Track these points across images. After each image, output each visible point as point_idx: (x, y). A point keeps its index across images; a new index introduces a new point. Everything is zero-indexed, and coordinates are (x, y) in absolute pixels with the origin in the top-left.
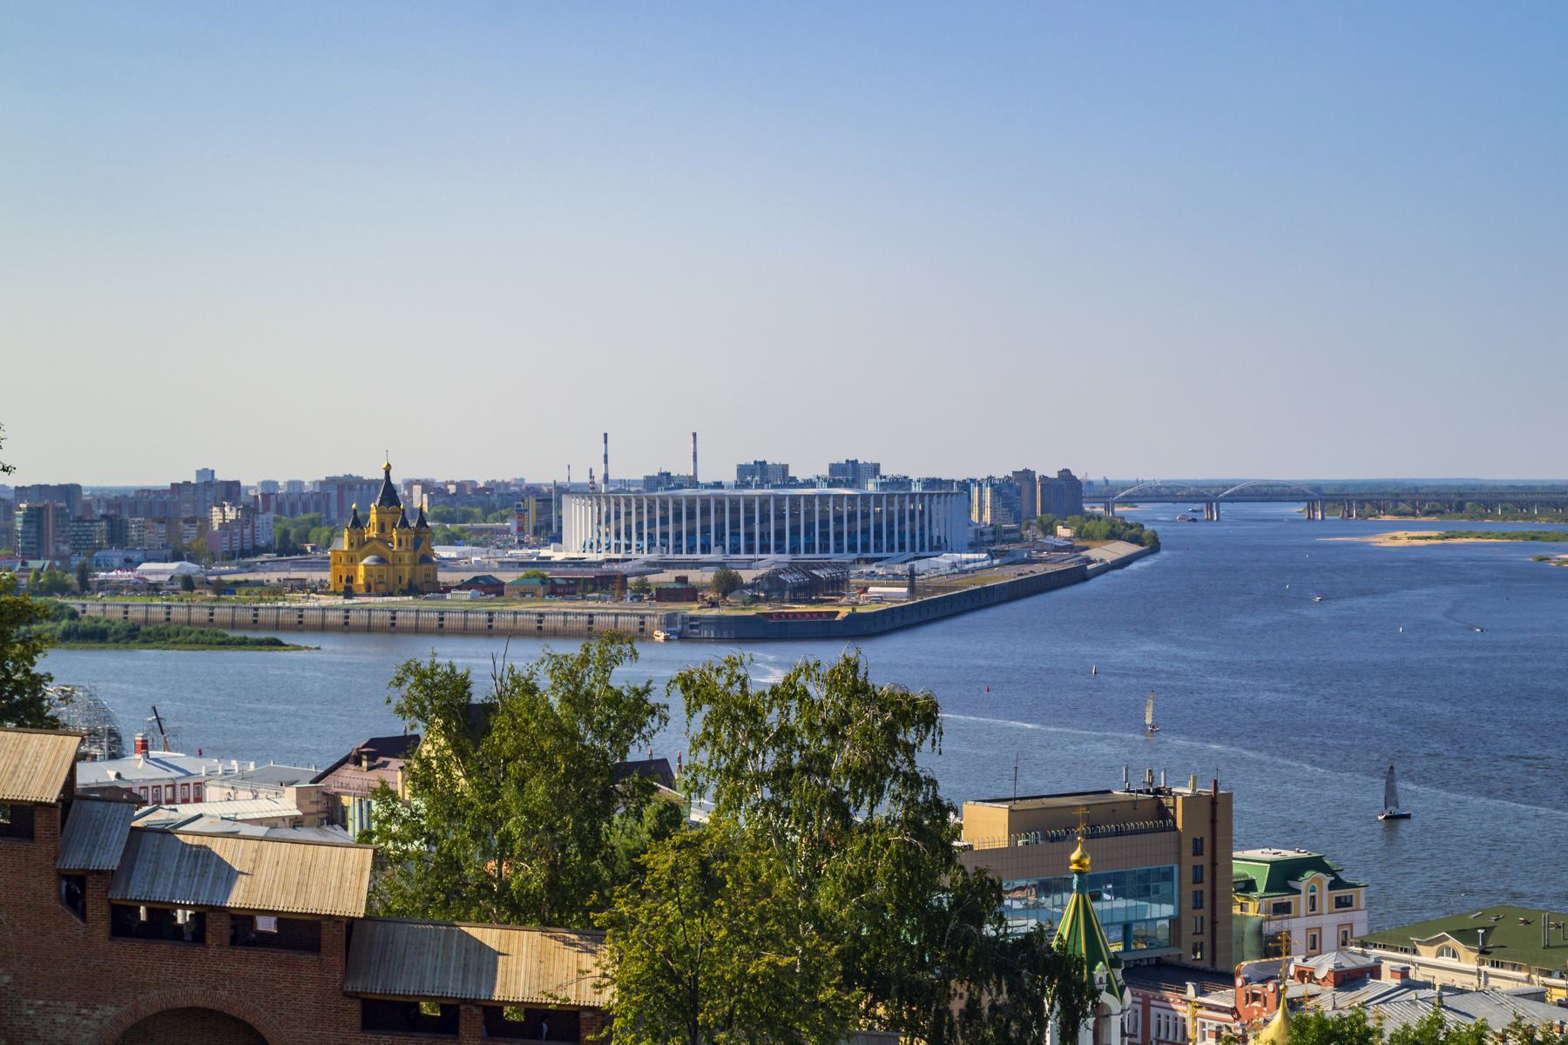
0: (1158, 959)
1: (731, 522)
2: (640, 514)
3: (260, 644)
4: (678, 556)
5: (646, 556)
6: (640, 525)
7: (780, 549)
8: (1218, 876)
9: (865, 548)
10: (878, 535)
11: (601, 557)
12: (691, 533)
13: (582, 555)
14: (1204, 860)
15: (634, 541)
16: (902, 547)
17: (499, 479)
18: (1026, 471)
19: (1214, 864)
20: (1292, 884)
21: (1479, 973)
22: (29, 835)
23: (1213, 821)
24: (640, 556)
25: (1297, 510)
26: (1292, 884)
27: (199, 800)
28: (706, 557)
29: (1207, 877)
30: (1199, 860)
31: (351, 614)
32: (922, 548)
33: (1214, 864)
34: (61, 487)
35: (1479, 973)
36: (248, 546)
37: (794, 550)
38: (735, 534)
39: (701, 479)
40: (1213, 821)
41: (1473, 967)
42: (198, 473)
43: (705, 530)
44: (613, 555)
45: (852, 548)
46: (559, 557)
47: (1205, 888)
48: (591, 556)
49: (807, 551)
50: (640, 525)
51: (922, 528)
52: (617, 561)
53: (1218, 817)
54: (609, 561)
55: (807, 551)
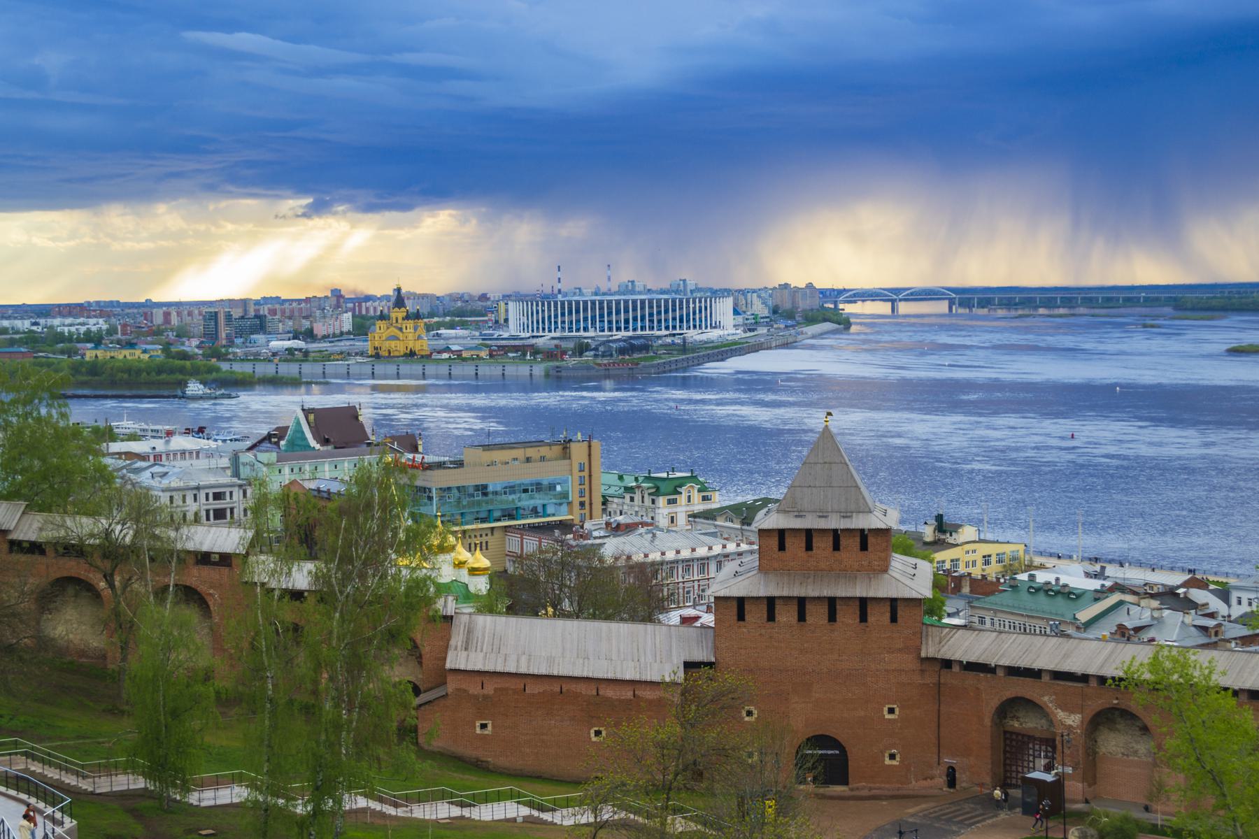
2: (549, 310)
3: (168, 397)
5: (553, 334)
7: (626, 328)
9: (674, 328)
10: (681, 321)
12: (578, 321)
14: (586, 474)
16: (695, 327)
17: (91, 300)
19: (590, 476)
22: (230, 565)
23: (590, 455)
25: (943, 307)
29: (587, 482)
33: (590, 476)
36: (337, 332)
37: (635, 330)
38: (602, 321)
40: (590, 455)
45: (667, 328)
46: (506, 335)
47: (586, 487)
48: (523, 335)
50: (550, 317)
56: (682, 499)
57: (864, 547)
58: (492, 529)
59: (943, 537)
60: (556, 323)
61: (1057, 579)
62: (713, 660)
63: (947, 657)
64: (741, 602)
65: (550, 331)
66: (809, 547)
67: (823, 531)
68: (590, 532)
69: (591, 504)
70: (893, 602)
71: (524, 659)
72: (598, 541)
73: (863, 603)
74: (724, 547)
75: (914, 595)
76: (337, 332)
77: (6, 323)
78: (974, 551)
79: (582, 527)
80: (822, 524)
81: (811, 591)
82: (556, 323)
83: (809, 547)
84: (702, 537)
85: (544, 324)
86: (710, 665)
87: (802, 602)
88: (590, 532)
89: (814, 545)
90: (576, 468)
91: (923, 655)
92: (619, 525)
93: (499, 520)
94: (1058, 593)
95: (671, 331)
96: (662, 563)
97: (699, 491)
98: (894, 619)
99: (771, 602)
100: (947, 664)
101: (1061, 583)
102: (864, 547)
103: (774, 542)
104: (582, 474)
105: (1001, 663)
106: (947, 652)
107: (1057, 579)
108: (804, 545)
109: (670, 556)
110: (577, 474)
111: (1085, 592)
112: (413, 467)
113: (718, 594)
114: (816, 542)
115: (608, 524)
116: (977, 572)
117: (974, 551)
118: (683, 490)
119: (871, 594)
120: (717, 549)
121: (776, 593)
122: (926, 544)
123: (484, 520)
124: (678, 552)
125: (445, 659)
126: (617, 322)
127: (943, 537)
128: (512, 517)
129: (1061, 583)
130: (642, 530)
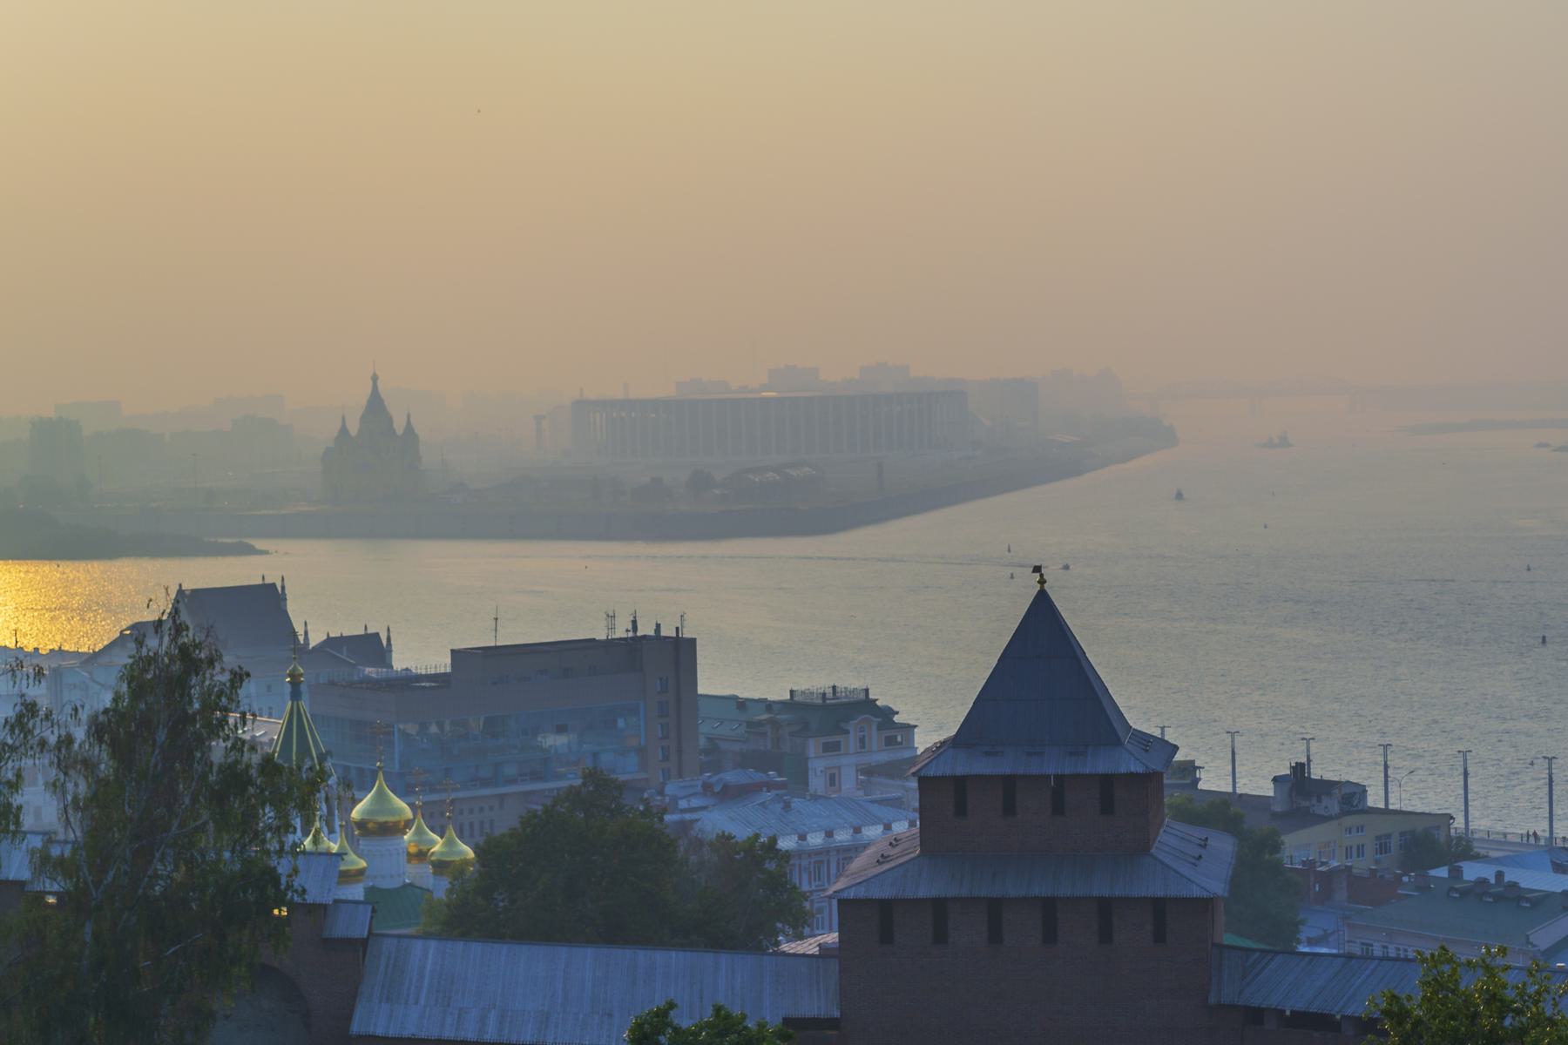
20: (843, 725)
26: (843, 725)
56: (851, 742)
57: (1107, 807)
58: (502, 797)
59: (1306, 804)
61: (1500, 875)
62: (837, 1014)
63: (1256, 1002)
64: (885, 907)
66: (1009, 809)
68: (675, 799)
70: (1159, 906)
71: (493, 1016)
72: (688, 816)
73: (1105, 907)
75: (1196, 892)
77: (1564, 664)
78: (1360, 829)
79: (661, 793)
80: (1035, 767)
81: (1011, 887)
83: (1009, 809)
84: (875, 808)
86: (832, 1023)
87: (995, 907)
88: (675, 799)
91: (1212, 1000)
92: (726, 787)
93: (512, 781)
94: (1499, 898)
96: (800, 853)
97: (880, 728)
98: (1159, 936)
99: (939, 906)
100: (1256, 1015)
101: (1507, 879)
102: (1107, 807)
105: (1349, 1012)
106: (1258, 996)
107: (1500, 875)
109: (816, 840)
111: (1549, 895)
113: (845, 895)
115: (707, 787)
116: (1361, 865)
117: (1360, 829)
118: (851, 726)
119: (1118, 892)
121: (952, 892)
122: (1275, 815)
123: (485, 783)
124: (829, 834)
125: (349, 1017)
127: (1306, 804)
128: (536, 776)
129: (1507, 879)
130: (767, 796)
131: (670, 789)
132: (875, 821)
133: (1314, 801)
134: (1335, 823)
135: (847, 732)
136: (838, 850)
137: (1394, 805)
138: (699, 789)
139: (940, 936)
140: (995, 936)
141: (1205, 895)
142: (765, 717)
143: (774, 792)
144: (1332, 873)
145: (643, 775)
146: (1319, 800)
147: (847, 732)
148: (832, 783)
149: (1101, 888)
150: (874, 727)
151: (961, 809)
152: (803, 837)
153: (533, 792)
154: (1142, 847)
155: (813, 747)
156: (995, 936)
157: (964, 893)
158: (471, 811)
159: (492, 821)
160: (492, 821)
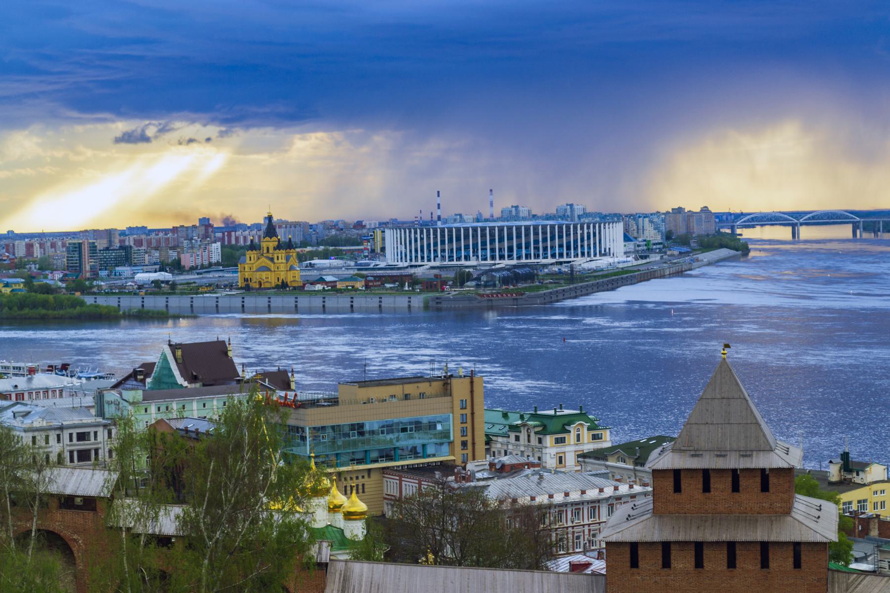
0: (441, 462)
1: (534, 241)
4: (529, 261)
6: (429, 245)
7: (510, 257)
8: (475, 420)
9: (561, 255)
11: (406, 264)
13: (396, 263)
14: (468, 411)
15: (524, 252)
16: (583, 254)
18: (680, 208)
19: (473, 414)
20: (567, 428)
21: (635, 470)
23: (472, 392)
24: (429, 263)
26: (567, 428)
27: (303, 430)
28: (561, 260)
30: (464, 412)
31: (219, 300)
32: (595, 255)
33: (473, 414)
34: (106, 230)
35: (635, 470)
36: (206, 263)
37: (519, 258)
38: (484, 249)
39: (523, 212)
40: (472, 392)
41: (631, 467)
42: (200, 220)
43: (467, 247)
44: (413, 263)
45: (553, 256)
47: (469, 425)
48: (401, 264)
49: (527, 258)
51: (595, 244)
52: (416, 266)
53: (475, 389)
54: (411, 266)
55: (527, 258)
56: (571, 438)
57: (765, 487)
58: (369, 470)
60: (435, 251)
65: (429, 260)
66: (706, 489)
67: (721, 471)
68: (473, 473)
69: (473, 444)
70: (797, 546)
72: (481, 483)
73: (765, 547)
74: (616, 488)
75: (819, 539)
76: (206, 263)
80: (721, 464)
81: (709, 535)
82: (435, 251)
83: (706, 489)
84: (593, 479)
85: (422, 252)
87: (699, 547)
89: (683, 487)
90: (457, 405)
92: (503, 466)
93: (376, 461)
95: (557, 259)
97: (589, 429)
98: (797, 564)
99: (666, 546)
102: (765, 487)
103: (669, 483)
104: (464, 412)
108: (700, 486)
109: (559, 498)
110: (458, 411)
112: (285, 405)
113: (610, 539)
114: (715, 483)
115: (492, 465)
118: (572, 428)
119: (773, 538)
120: (609, 492)
122: (831, 484)
123: (360, 462)
124: (567, 495)
126: (500, 250)
130: (528, 471)
131: (470, 466)
132: (594, 486)
133: (855, 474)
134: (867, 488)
135: (570, 432)
136: (572, 504)
137: (401, 386)
138: (487, 467)
139: (666, 564)
140: (699, 564)
141: (825, 540)
142: (519, 422)
143: (532, 469)
144: (869, 519)
145: (452, 458)
146: (858, 475)
147: (570, 432)
148: (561, 462)
149: (760, 535)
150: (585, 429)
151: (677, 489)
152: (551, 496)
153: (388, 468)
154: (787, 511)
155: (549, 440)
156: (699, 564)
157: (681, 538)
158: (351, 479)
159: (363, 485)
160: (363, 485)
